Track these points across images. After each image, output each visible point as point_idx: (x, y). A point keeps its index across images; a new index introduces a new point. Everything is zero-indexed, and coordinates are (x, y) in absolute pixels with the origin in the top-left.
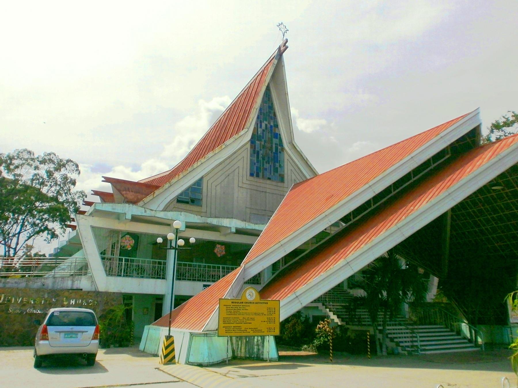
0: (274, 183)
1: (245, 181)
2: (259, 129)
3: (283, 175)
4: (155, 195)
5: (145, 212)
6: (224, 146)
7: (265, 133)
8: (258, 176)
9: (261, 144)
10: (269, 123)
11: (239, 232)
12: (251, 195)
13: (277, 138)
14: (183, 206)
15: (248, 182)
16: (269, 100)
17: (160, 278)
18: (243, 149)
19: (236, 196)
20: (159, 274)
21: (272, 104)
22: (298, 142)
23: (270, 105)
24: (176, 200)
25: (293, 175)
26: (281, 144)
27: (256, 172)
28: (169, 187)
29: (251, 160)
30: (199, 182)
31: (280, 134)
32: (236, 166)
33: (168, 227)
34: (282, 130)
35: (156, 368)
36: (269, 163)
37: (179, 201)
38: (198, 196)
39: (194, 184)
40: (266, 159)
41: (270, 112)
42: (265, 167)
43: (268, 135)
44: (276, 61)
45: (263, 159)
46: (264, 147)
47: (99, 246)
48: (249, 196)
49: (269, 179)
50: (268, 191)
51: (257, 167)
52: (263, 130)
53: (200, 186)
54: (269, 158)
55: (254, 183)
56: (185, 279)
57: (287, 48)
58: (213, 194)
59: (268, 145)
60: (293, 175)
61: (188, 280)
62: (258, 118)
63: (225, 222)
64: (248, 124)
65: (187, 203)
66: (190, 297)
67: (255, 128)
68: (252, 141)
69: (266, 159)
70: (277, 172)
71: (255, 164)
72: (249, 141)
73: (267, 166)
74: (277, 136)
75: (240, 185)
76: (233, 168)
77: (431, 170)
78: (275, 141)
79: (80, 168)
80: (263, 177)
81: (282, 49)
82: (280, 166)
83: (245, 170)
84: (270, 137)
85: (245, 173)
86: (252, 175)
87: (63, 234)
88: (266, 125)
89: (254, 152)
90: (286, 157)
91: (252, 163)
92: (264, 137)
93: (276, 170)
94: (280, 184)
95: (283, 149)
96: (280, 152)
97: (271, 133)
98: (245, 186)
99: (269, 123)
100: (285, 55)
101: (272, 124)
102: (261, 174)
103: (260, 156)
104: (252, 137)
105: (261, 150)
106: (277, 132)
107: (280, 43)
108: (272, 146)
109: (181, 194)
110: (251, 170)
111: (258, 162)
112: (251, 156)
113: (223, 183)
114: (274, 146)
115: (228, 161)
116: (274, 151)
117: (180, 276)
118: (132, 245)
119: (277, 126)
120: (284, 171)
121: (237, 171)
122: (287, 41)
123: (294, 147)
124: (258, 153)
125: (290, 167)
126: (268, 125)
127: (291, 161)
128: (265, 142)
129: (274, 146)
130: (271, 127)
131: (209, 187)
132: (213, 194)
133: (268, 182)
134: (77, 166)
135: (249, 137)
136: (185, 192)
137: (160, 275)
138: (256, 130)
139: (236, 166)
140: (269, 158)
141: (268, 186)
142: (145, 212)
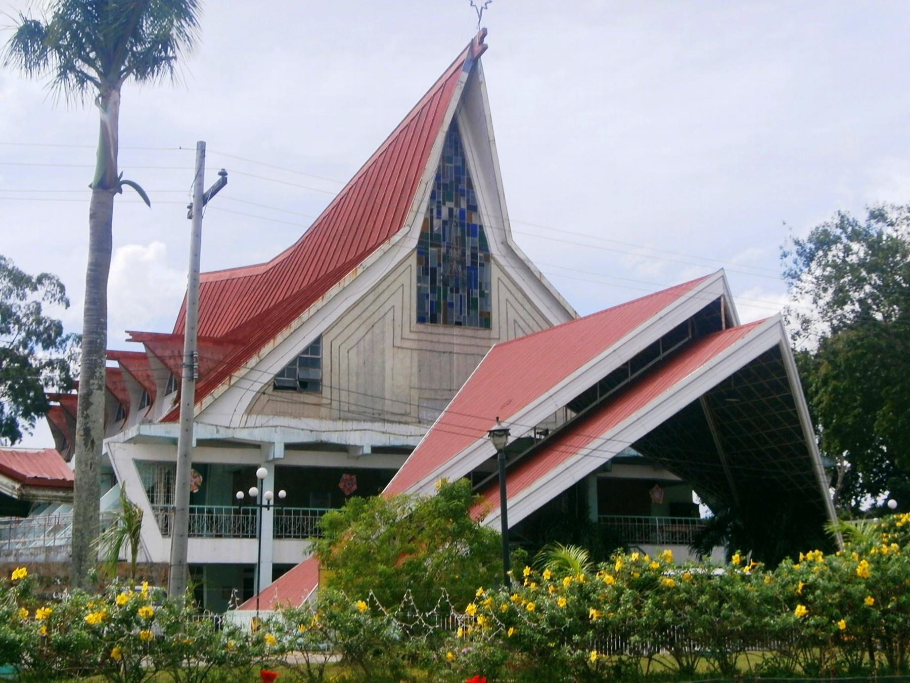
0: (469, 332)
1: (407, 334)
2: (436, 222)
3: (489, 314)
4: (233, 382)
5: (218, 431)
6: (360, 271)
7: (447, 228)
8: (434, 320)
9: (439, 251)
10: (457, 204)
11: (376, 450)
12: (419, 361)
13: (474, 235)
14: (287, 395)
15: (413, 336)
16: (456, 155)
17: (247, 537)
18: (401, 268)
19: (388, 366)
20: (246, 528)
21: (464, 161)
22: (521, 241)
23: (460, 164)
24: (271, 388)
25: (510, 310)
26: (484, 244)
27: (431, 312)
28: (257, 364)
29: (419, 289)
30: (315, 346)
31: (481, 227)
32: (387, 306)
33: (258, 451)
34: (486, 218)
35: (223, 174)
36: (457, 292)
37: (276, 388)
38: (311, 374)
39: (306, 351)
40: (452, 284)
41: (458, 180)
42: (449, 300)
43: (456, 232)
44: (464, 76)
45: (446, 284)
46: (446, 258)
47: (144, 481)
48: (415, 364)
49: (459, 324)
50: (456, 349)
51: (432, 302)
52: (445, 223)
53: (318, 354)
54: (457, 281)
55: (423, 337)
56: (290, 537)
57: (485, 48)
58: (344, 366)
59: (455, 254)
60: (510, 310)
61: (295, 537)
62: (433, 196)
63: (352, 439)
64: (410, 217)
65: (294, 389)
66: (295, 565)
67: (425, 220)
68: (421, 250)
69: (452, 284)
70: (475, 307)
71: (428, 295)
72: (413, 250)
73: (454, 298)
74: (477, 232)
75: (398, 343)
76: (382, 311)
77: (659, 361)
78: (469, 240)
79: (68, 294)
80: (445, 322)
81: (477, 48)
82: (482, 294)
83: (406, 313)
84: (459, 234)
85: (406, 317)
86: (421, 320)
87: (31, 430)
88: (451, 211)
89: (426, 271)
90: (495, 273)
91: (421, 297)
92: (447, 235)
93: (473, 304)
94: (482, 333)
95: (488, 257)
96: (482, 265)
97: (462, 225)
98: (407, 344)
99: (457, 204)
100: (485, 60)
101: (464, 205)
102: (441, 316)
103: (439, 278)
104: (420, 242)
105: (439, 265)
106: (474, 222)
107: (474, 33)
108: (464, 254)
109: (281, 374)
110: (420, 306)
111: (433, 290)
112: (419, 280)
113: (362, 342)
114: (468, 253)
115: (371, 297)
116: (468, 264)
117: (280, 532)
118: (199, 484)
119: (473, 208)
120: (491, 305)
121: (389, 316)
122: (484, 33)
123: (511, 252)
124: (434, 270)
125: (504, 294)
126: (455, 209)
127: (506, 281)
128: (449, 247)
129: (468, 253)
130: (462, 213)
131: (335, 354)
132: (344, 366)
133: (456, 330)
134: (62, 288)
135: (413, 243)
136: (289, 370)
137: (247, 532)
138: (428, 223)
139: (387, 306)
140: (457, 281)
141: (455, 340)
142: (218, 431)
